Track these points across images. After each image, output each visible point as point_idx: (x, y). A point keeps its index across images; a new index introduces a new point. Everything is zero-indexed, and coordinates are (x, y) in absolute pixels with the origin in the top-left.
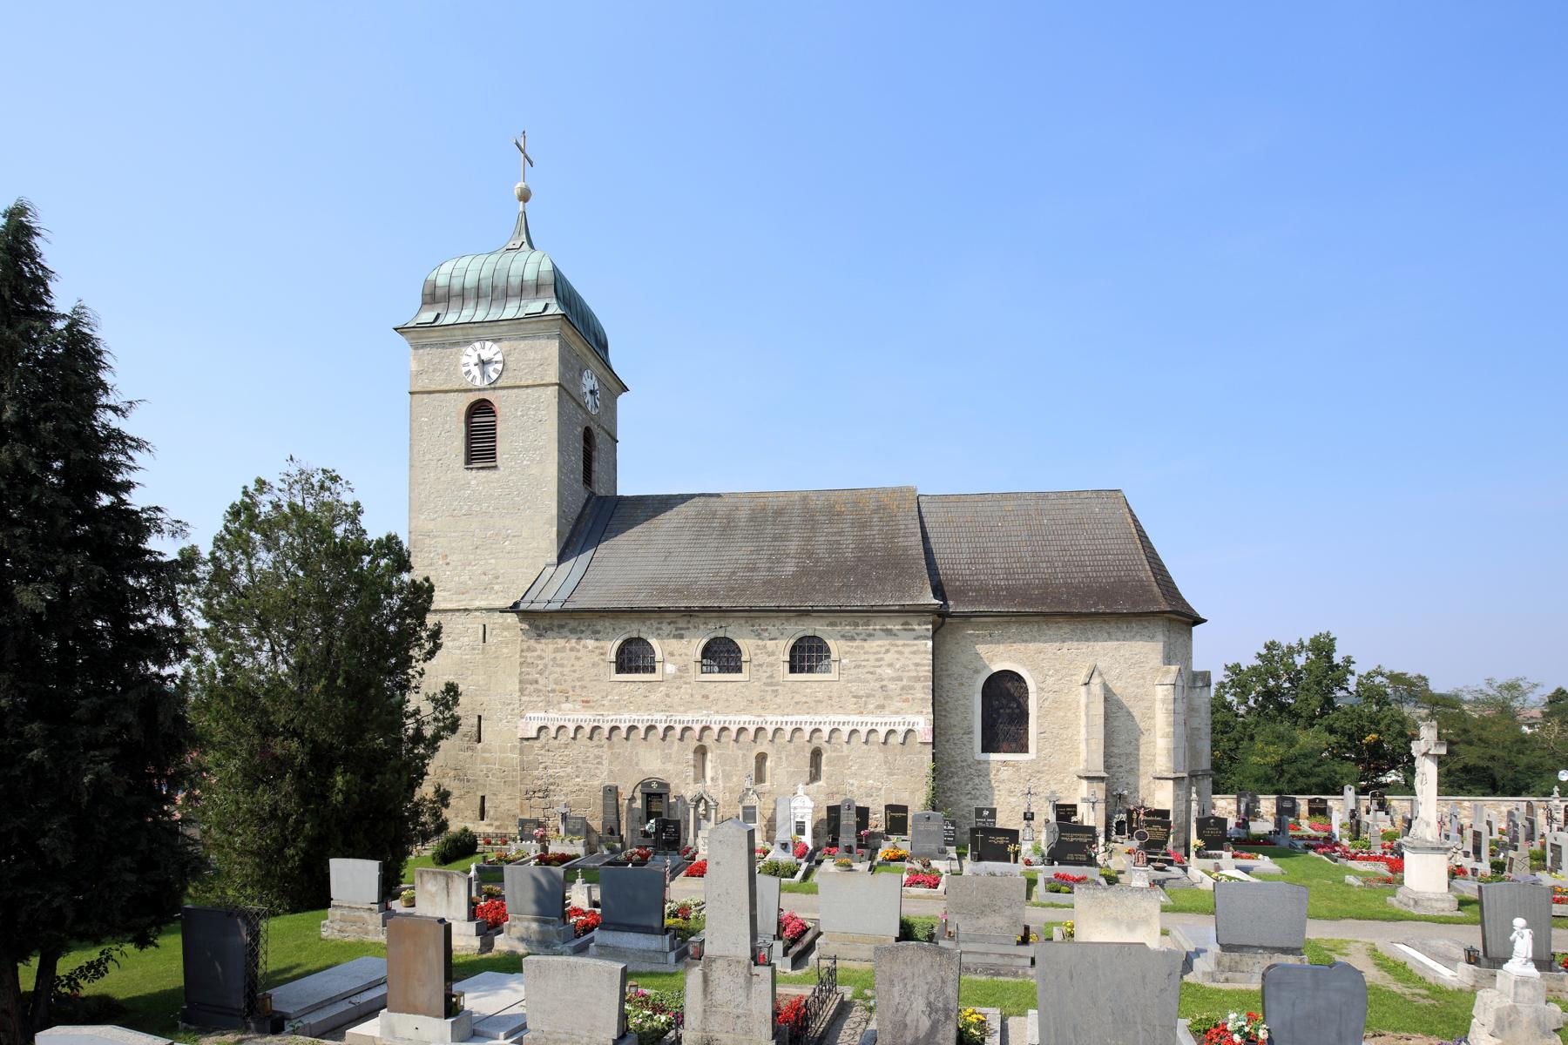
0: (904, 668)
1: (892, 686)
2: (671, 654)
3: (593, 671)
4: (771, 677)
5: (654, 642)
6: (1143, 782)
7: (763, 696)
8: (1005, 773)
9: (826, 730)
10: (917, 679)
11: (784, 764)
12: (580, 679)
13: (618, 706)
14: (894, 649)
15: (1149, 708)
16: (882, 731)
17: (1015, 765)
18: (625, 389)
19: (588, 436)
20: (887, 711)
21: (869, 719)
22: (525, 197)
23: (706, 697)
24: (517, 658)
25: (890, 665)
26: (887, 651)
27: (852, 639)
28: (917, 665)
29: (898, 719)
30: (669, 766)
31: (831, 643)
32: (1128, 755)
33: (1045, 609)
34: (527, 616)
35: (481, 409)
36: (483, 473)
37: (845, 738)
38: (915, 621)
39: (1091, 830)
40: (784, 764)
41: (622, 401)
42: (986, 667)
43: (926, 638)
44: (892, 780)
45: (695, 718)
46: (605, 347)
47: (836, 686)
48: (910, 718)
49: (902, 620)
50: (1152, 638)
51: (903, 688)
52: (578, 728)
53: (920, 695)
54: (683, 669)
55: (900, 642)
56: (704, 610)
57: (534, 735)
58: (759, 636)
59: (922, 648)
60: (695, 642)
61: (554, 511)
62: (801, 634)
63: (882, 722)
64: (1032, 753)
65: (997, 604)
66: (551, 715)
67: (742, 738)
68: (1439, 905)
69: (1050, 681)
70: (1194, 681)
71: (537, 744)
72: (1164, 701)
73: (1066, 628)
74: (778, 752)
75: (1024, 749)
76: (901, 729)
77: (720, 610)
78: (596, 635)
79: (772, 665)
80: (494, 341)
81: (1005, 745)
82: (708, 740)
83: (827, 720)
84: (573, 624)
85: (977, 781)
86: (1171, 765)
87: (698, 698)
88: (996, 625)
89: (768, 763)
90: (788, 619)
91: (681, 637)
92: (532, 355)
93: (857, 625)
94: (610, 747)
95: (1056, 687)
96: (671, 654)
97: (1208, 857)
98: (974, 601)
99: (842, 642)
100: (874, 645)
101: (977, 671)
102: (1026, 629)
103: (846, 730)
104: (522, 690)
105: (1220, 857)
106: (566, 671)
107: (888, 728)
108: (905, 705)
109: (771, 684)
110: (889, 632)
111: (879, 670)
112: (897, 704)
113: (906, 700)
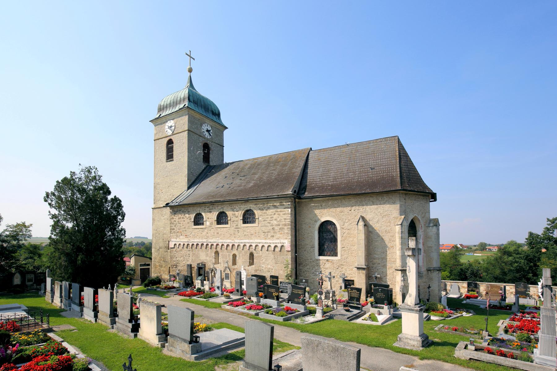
0: (280, 221)
1: (276, 228)
2: (208, 218)
3: (188, 225)
4: (237, 225)
5: (203, 214)
6: (389, 272)
7: (234, 234)
8: (328, 265)
9: (254, 245)
10: (285, 225)
11: (241, 258)
12: (185, 228)
13: (194, 237)
14: (277, 213)
15: (393, 236)
16: (273, 246)
17: (332, 261)
18: (226, 128)
19: (206, 146)
20: (275, 238)
21: (268, 241)
22: (190, 70)
23: (218, 233)
24: (169, 222)
25: (276, 220)
26: (275, 214)
27: (263, 210)
28: (285, 219)
29: (278, 241)
30: (208, 258)
31: (255, 212)
32: (383, 259)
33: (343, 193)
34: (172, 207)
35: (170, 142)
36: (170, 162)
37: (260, 248)
38: (285, 201)
39: (359, 290)
40: (241, 258)
41: (226, 132)
42: (319, 219)
43: (288, 208)
44: (277, 267)
45: (214, 241)
46: (218, 115)
47: (257, 228)
48: (282, 241)
49: (280, 201)
50: (394, 203)
51: (280, 229)
52: (223, 245)
53: (286, 231)
54: (211, 224)
55: (279, 210)
56: (216, 202)
57: (173, 247)
58: (233, 211)
59: (287, 212)
60: (215, 213)
61: (187, 173)
62: (246, 209)
63: (273, 242)
64: (339, 257)
65: (323, 192)
66: (177, 240)
67: (228, 248)
68: (412, 343)
69: (346, 224)
70: (429, 223)
71: (174, 250)
72: (398, 232)
73: (353, 201)
74: (239, 254)
75: (336, 255)
76: (279, 245)
77: (219, 202)
78: (189, 213)
79: (237, 221)
80: (173, 119)
81: (329, 253)
82: (219, 249)
83: (254, 241)
84: (183, 209)
85: (316, 268)
86: (401, 264)
87: (216, 233)
88: (323, 201)
89: (237, 258)
90: (242, 203)
91: (211, 212)
92: (181, 122)
93: (264, 204)
94: (192, 251)
95: (349, 228)
96: (208, 218)
97: (376, 307)
98: (317, 191)
99: (259, 211)
100: (270, 212)
101: (316, 221)
102: (336, 202)
103: (260, 245)
104: (171, 232)
105: (383, 308)
106: (181, 225)
107: (275, 245)
108: (281, 235)
109: (237, 228)
110: (275, 207)
111: (272, 222)
112: (278, 235)
113: (281, 234)
